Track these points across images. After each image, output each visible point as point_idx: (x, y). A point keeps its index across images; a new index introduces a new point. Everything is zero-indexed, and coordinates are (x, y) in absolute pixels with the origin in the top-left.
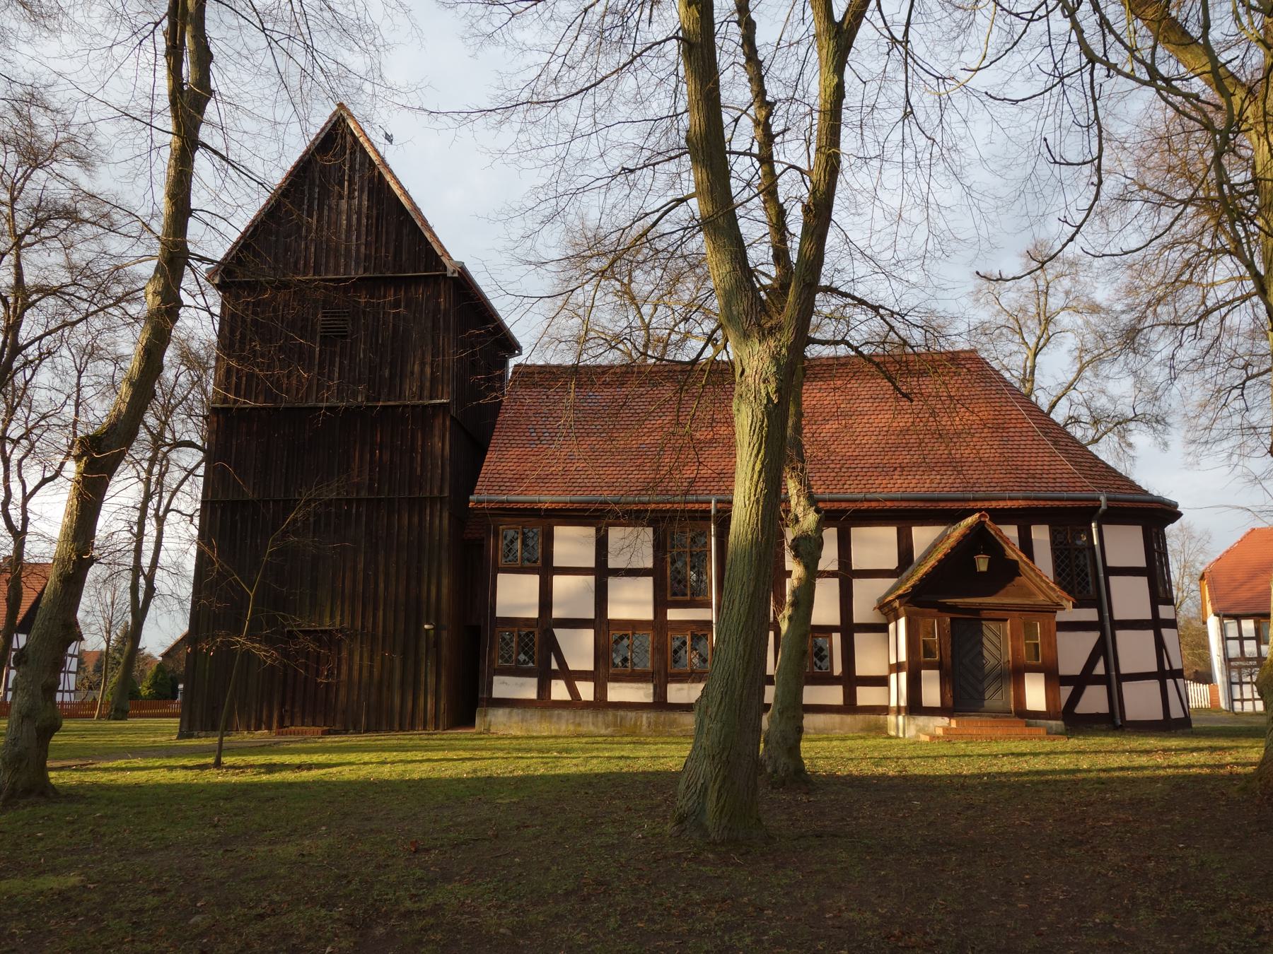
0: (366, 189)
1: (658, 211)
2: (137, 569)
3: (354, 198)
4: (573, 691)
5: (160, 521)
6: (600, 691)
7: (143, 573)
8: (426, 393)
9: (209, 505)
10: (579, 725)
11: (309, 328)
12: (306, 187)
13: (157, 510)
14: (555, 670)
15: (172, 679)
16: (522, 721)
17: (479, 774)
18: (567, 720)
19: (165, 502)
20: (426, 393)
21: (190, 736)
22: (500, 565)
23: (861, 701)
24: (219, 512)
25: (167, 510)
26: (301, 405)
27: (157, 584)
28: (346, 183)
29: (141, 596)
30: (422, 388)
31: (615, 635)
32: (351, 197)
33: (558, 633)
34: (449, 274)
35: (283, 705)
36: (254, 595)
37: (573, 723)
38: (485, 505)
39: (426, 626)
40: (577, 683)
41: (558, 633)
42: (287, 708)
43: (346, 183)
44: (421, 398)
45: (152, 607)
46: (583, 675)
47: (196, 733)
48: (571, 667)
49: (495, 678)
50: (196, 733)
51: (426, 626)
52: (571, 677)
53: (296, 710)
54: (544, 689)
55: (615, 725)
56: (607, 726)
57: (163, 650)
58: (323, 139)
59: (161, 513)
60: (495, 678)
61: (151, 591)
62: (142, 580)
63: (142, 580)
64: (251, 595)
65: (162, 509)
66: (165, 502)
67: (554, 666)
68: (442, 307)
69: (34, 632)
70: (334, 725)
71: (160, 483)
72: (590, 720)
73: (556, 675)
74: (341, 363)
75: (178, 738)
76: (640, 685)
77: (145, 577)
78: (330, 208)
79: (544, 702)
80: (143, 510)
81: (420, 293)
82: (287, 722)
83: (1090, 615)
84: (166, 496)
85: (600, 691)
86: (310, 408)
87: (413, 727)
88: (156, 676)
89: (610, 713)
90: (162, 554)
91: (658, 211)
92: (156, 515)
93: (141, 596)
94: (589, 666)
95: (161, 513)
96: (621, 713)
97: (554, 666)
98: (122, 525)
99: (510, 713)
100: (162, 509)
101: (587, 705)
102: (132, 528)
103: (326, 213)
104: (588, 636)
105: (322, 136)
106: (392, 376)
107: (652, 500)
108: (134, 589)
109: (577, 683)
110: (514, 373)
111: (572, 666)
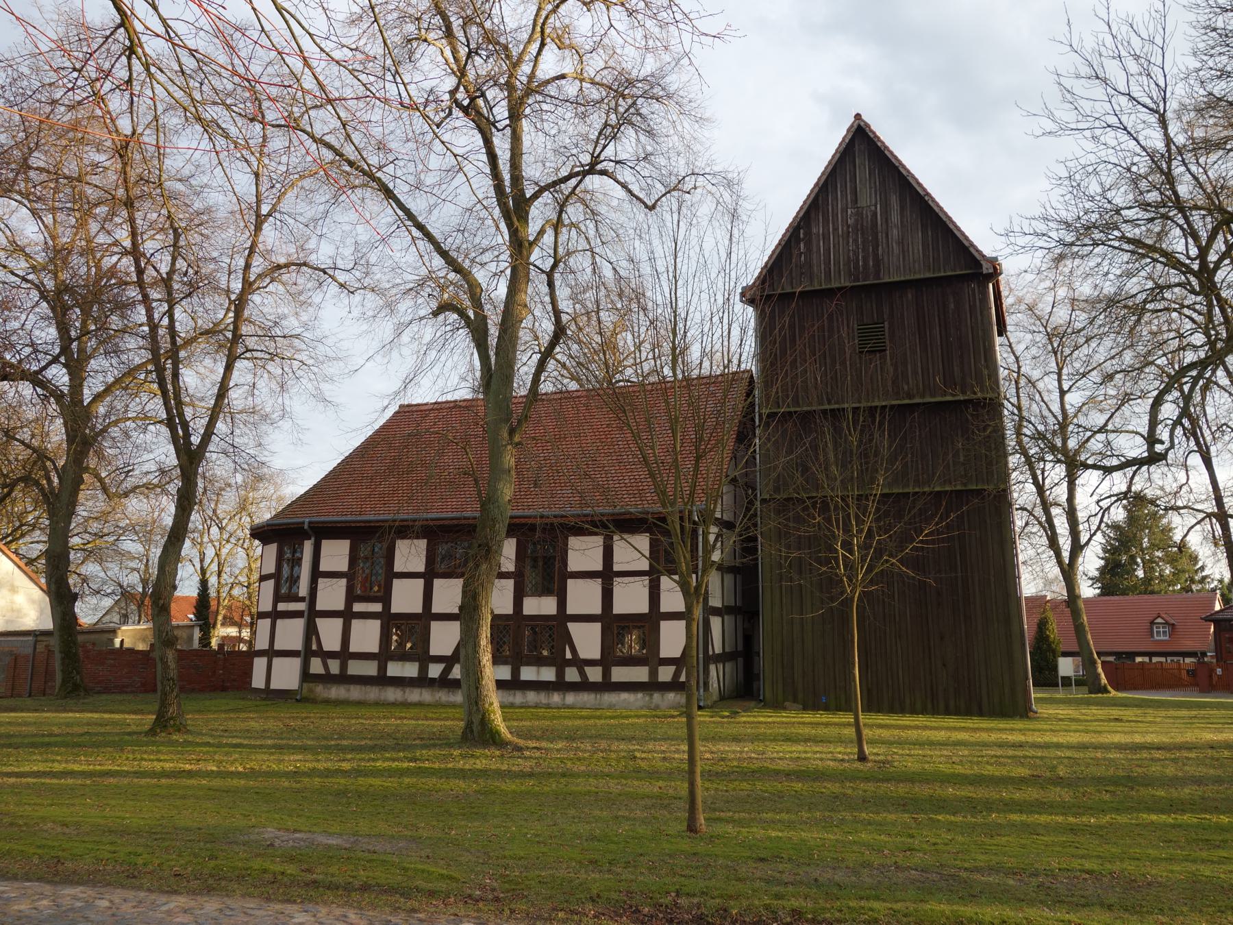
1: (286, 22)
4: (582, 673)
6: (606, 674)
17: (498, 753)
23: (712, 668)
48: (678, 655)
52: (581, 664)
54: (560, 674)
64: (841, 551)
67: (569, 655)
69: (462, 660)
73: (570, 663)
79: (560, 685)
83: (377, 607)
85: (606, 674)
90: (527, 160)
91: (286, 22)
97: (569, 655)
107: (650, 504)
110: (971, 269)
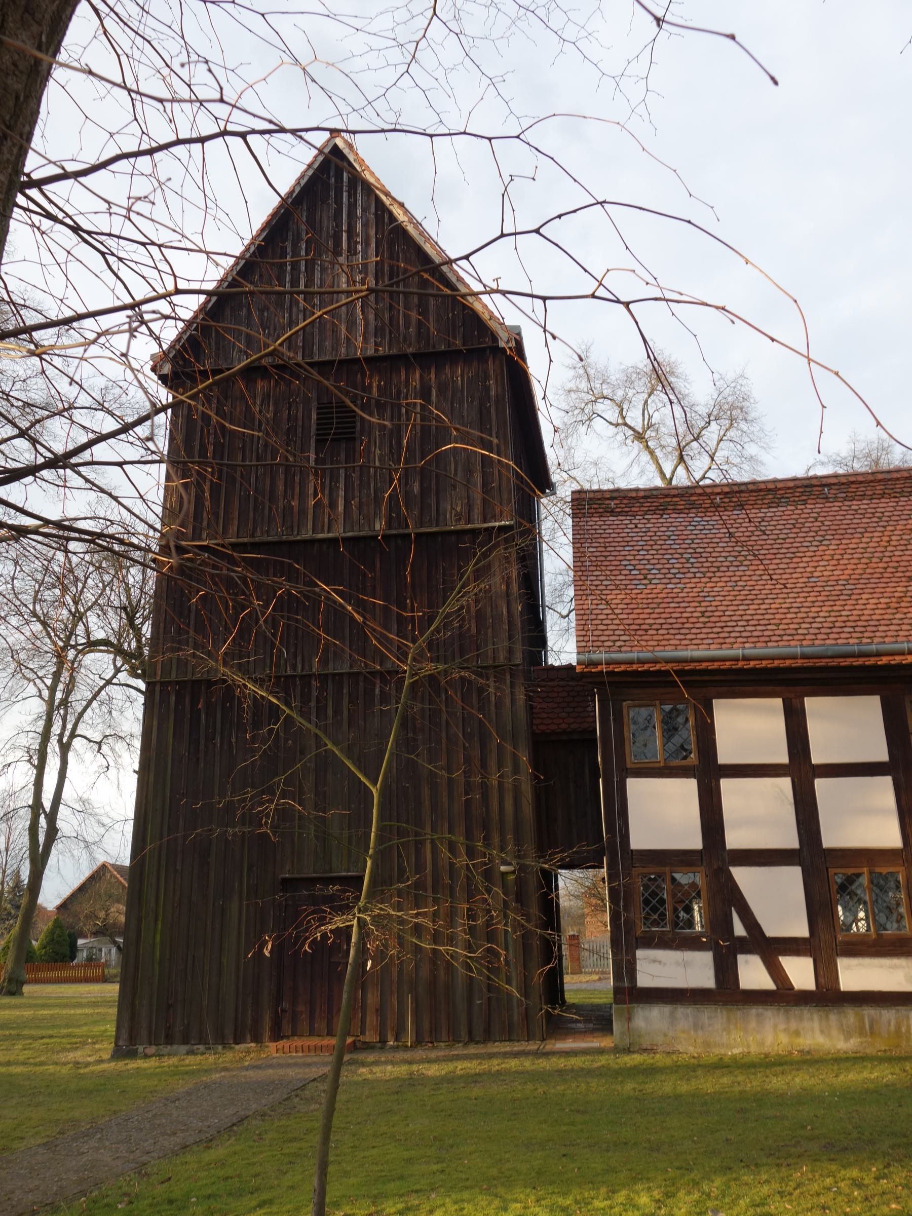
0: (373, 241)
2: (37, 806)
3: (356, 253)
5: (65, 748)
7: (44, 812)
8: (477, 511)
9: (158, 688)
10: (797, 1033)
11: (299, 430)
12: (289, 244)
13: (61, 736)
14: (741, 939)
15: (70, 936)
16: (696, 1027)
18: (775, 1026)
19: (69, 726)
20: (477, 511)
21: (132, 1054)
22: (629, 765)
24: (173, 698)
25: (73, 735)
26: (292, 538)
27: (60, 824)
28: (344, 235)
29: (42, 838)
30: (470, 507)
31: (838, 876)
32: (352, 251)
33: (742, 875)
34: (502, 344)
35: (278, 999)
36: (382, 794)
37: (785, 1030)
38: (604, 668)
39: (503, 868)
40: (782, 959)
41: (742, 875)
42: (285, 1005)
43: (344, 235)
44: (469, 521)
45: (54, 851)
46: (793, 946)
47: (141, 1049)
49: (640, 953)
50: (141, 1049)
51: (503, 868)
53: (301, 1008)
55: (861, 1032)
56: (848, 1036)
57: (58, 902)
58: (311, 177)
59: (65, 740)
60: (640, 953)
61: (52, 832)
62: (43, 821)
63: (43, 821)
65: (67, 733)
66: (69, 726)
67: (739, 930)
68: (493, 393)
70: (363, 1033)
71: (65, 702)
72: (816, 1025)
73: (744, 946)
74: (347, 477)
75: (119, 1054)
76: (895, 961)
77: (47, 816)
78: (323, 270)
80: (45, 736)
81: (459, 375)
82: (287, 1029)
84: (71, 720)
86: (305, 542)
87: (488, 1037)
88: (52, 932)
89: (851, 1015)
92: (60, 741)
93: (42, 838)
94: (802, 930)
95: (65, 740)
96: (869, 1012)
97: (739, 930)
98: (19, 754)
99: (672, 1015)
100: (67, 733)
101: (804, 998)
102: (31, 757)
103: (317, 274)
104: (792, 876)
105: (310, 172)
106: (424, 491)
108: (33, 829)
109: (782, 959)
111: (771, 930)
